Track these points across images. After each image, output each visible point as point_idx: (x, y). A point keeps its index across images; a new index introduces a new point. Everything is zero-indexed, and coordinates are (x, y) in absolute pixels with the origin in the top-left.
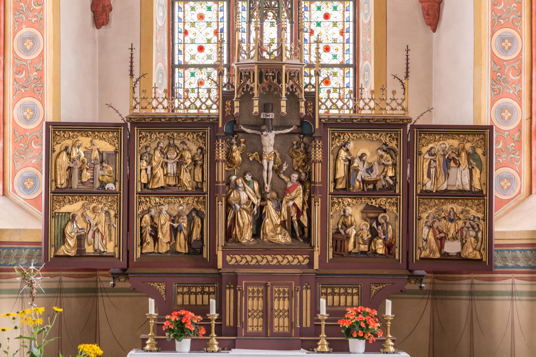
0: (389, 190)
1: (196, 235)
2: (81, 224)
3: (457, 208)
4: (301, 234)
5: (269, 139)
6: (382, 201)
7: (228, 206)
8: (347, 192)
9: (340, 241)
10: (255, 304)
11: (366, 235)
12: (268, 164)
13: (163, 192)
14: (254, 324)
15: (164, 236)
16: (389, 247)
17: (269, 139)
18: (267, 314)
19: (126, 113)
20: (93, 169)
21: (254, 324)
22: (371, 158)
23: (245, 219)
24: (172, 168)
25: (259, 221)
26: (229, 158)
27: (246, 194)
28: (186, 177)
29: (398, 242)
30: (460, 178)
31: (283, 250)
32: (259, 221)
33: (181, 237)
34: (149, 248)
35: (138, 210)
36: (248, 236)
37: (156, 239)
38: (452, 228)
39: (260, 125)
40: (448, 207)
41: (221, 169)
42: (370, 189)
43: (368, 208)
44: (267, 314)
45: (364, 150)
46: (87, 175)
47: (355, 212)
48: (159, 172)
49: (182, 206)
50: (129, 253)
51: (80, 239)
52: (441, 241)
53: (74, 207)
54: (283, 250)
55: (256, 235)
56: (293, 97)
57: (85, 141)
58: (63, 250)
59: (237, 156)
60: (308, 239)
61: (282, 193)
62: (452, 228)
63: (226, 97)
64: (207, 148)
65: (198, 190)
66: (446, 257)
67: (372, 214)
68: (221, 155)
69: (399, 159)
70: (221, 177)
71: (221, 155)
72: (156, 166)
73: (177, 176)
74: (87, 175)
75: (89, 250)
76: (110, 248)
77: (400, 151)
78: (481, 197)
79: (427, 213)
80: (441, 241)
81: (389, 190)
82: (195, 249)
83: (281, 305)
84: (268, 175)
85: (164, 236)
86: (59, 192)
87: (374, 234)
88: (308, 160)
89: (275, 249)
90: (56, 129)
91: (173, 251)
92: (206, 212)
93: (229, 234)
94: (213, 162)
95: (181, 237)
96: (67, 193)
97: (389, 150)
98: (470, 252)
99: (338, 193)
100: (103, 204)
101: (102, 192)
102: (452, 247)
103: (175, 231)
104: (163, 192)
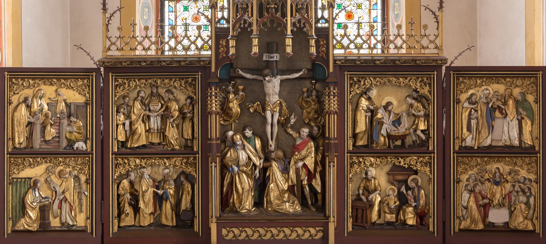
0: (420, 147)
1: (185, 204)
2: (45, 192)
3: (504, 168)
4: (313, 201)
5: (273, 86)
6: (412, 160)
7: (224, 168)
9: (361, 208)
11: (393, 202)
12: (272, 116)
13: (145, 152)
15: (146, 206)
16: (421, 216)
17: (273, 86)
19: (99, 56)
20: (58, 124)
22: (398, 107)
23: (244, 183)
24: (155, 123)
25: (261, 185)
26: (225, 109)
27: (247, 153)
28: (172, 133)
29: (433, 210)
31: (290, 221)
33: (167, 207)
34: (128, 221)
35: (114, 174)
36: (248, 204)
37: (136, 210)
38: (498, 193)
39: (262, 69)
40: (493, 166)
41: (215, 124)
42: (398, 146)
43: (395, 169)
45: (390, 98)
46: (51, 132)
47: (379, 174)
48: (140, 128)
49: (167, 169)
50: (103, 224)
51: (44, 210)
52: (485, 209)
54: (290, 221)
55: (258, 203)
56: (300, 34)
57: (48, 90)
58: (23, 224)
59: (235, 106)
60: (322, 208)
62: (498, 193)
63: (220, 35)
64: (198, 97)
65: (187, 149)
66: (490, 228)
67: (400, 176)
68: (214, 106)
69: (433, 109)
70: (214, 132)
71: (214, 106)
72: (136, 121)
73: (162, 132)
74: (51, 132)
75: (55, 223)
76: (81, 221)
77: (434, 98)
79: (467, 176)
80: (485, 209)
82: (184, 220)
84: (272, 129)
85: (146, 206)
87: (403, 200)
88: (321, 112)
91: (157, 224)
92: (198, 176)
93: (225, 201)
94: (205, 115)
95: (167, 207)
97: (420, 98)
99: (358, 151)
100: (70, 167)
101: (70, 152)
102: (498, 216)
103: (159, 199)
104: (145, 152)
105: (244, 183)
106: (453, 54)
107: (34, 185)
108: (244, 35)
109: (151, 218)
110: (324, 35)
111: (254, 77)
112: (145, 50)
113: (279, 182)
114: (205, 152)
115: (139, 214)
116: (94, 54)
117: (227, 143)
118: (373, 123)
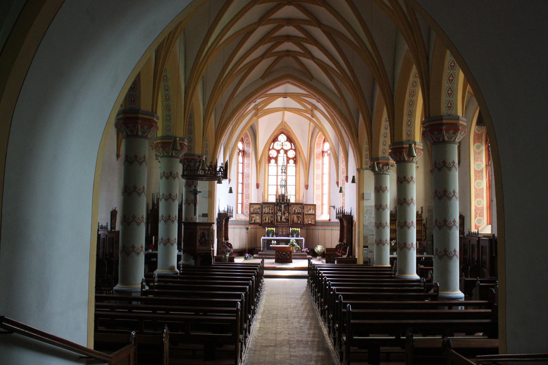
0: (300, 214)
5: (283, 206)
6: (299, 215)
8: (294, 214)
9: (293, 221)
10: (281, 230)
12: (283, 210)
13: (267, 213)
14: (280, 233)
15: (267, 220)
17: (283, 206)
18: (282, 232)
21: (280, 233)
23: (279, 218)
25: (281, 218)
27: (279, 214)
30: (311, 212)
32: (281, 218)
39: (281, 204)
42: (298, 213)
44: (282, 232)
47: (295, 217)
53: (254, 215)
56: (287, 200)
61: (284, 213)
63: (277, 199)
65: (272, 213)
67: (298, 217)
78: (314, 215)
81: (300, 214)
82: (272, 222)
83: (284, 230)
85: (267, 220)
86: (253, 213)
88: (289, 209)
89: (283, 222)
90: (251, 204)
96: (253, 213)
98: (313, 223)
101: (258, 213)
102: (310, 222)
104: (267, 213)
105: (279, 218)
106: (304, 203)
107: (253, 217)
108: (280, 200)
109: (477, 227)
110: (289, 200)
111: (357, 44)
112: (266, 201)
113: (283, 217)
114: (275, 214)
115: (147, 210)
116: (261, 202)
117: (277, 213)
118: (295, 211)
